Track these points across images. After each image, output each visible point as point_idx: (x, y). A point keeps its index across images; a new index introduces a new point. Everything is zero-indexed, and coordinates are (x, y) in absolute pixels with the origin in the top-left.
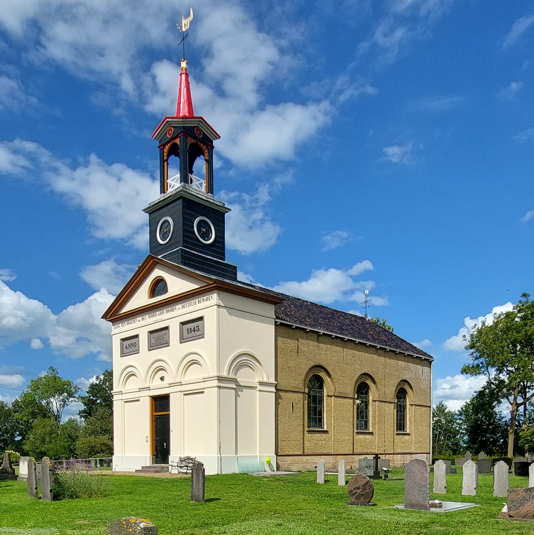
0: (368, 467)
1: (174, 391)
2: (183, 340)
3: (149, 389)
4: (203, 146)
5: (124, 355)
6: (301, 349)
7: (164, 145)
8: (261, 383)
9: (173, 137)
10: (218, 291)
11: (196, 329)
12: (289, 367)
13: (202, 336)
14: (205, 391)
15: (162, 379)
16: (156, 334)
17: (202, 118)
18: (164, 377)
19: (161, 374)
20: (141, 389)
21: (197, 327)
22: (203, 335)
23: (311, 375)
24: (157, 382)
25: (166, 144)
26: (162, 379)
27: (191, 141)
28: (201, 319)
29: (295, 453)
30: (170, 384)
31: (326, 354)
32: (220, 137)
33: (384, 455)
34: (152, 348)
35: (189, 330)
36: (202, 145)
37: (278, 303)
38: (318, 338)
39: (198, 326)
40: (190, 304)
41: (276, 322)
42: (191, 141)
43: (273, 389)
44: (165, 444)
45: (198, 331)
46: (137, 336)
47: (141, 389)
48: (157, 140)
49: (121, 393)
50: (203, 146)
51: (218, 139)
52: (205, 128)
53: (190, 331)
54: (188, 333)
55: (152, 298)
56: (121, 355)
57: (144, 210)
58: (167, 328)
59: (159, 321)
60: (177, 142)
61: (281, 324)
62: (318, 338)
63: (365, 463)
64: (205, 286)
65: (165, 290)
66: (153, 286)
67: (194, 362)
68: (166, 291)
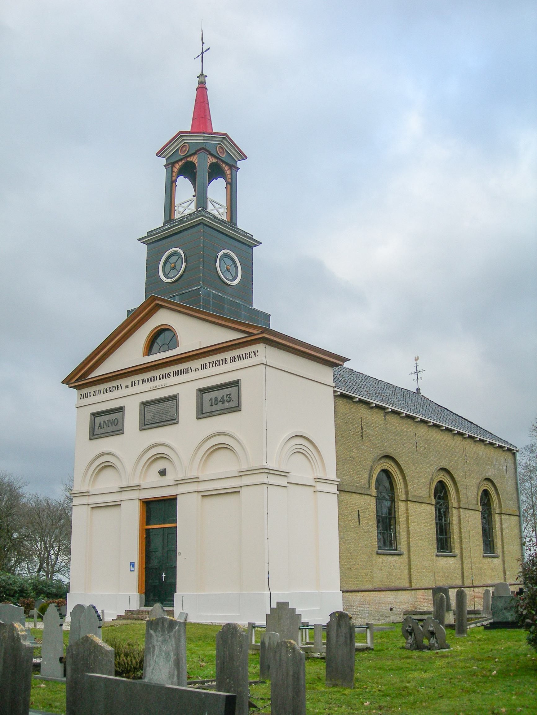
0: (509, 608)
1: (248, 483)
2: (202, 414)
3: (138, 488)
4: (225, 167)
5: (205, 415)
6: (365, 431)
7: (173, 164)
8: (319, 480)
9: (187, 155)
10: (265, 345)
11: (225, 398)
12: (352, 457)
13: (237, 408)
14: (122, 503)
15: (163, 473)
16: (153, 408)
17: (226, 135)
18: (160, 472)
19: (160, 465)
20: (123, 489)
21: (227, 395)
22: (121, 430)
23: (379, 470)
24: (153, 478)
25: (177, 162)
26: (163, 473)
27: (211, 161)
28: (236, 383)
29: (364, 588)
30: (121, 488)
31: (395, 440)
32: (246, 158)
33: (472, 589)
34: (201, 416)
35: (213, 400)
36: (224, 165)
37: (336, 365)
38: (385, 417)
39: (230, 394)
40: (216, 363)
41: (335, 392)
42: (211, 161)
43: (334, 489)
44: (164, 575)
45: (228, 402)
46: (121, 409)
47: (123, 489)
48: (164, 158)
49: (86, 494)
50: (225, 167)
51: (245, 160)
52: (228, 145)
53: (215, 401)
54: (212, 405)
55: (148, 355)
56: (197, 416)
57: (139, 240)
58: (175, 398)
59: (161, 387)
60: (195, 163)
61: (343, 396)
62: (385, 417)
63: (503, 602)
64: (247, 337)
65: (173, 342)
66: (149, 341)
67: (108, 466)
68: (176, 345)
